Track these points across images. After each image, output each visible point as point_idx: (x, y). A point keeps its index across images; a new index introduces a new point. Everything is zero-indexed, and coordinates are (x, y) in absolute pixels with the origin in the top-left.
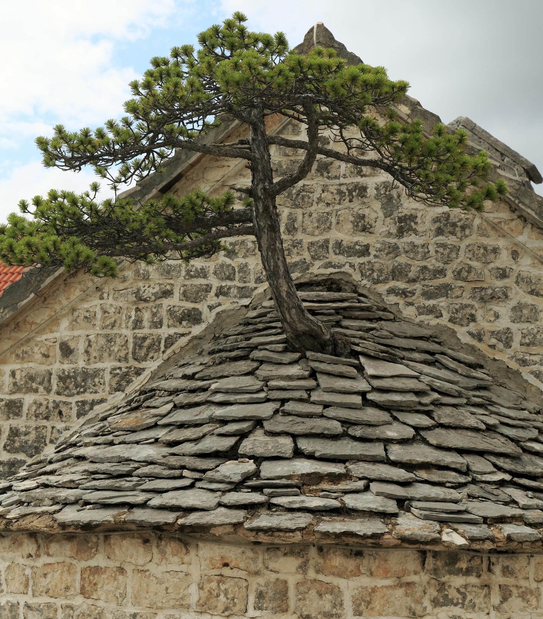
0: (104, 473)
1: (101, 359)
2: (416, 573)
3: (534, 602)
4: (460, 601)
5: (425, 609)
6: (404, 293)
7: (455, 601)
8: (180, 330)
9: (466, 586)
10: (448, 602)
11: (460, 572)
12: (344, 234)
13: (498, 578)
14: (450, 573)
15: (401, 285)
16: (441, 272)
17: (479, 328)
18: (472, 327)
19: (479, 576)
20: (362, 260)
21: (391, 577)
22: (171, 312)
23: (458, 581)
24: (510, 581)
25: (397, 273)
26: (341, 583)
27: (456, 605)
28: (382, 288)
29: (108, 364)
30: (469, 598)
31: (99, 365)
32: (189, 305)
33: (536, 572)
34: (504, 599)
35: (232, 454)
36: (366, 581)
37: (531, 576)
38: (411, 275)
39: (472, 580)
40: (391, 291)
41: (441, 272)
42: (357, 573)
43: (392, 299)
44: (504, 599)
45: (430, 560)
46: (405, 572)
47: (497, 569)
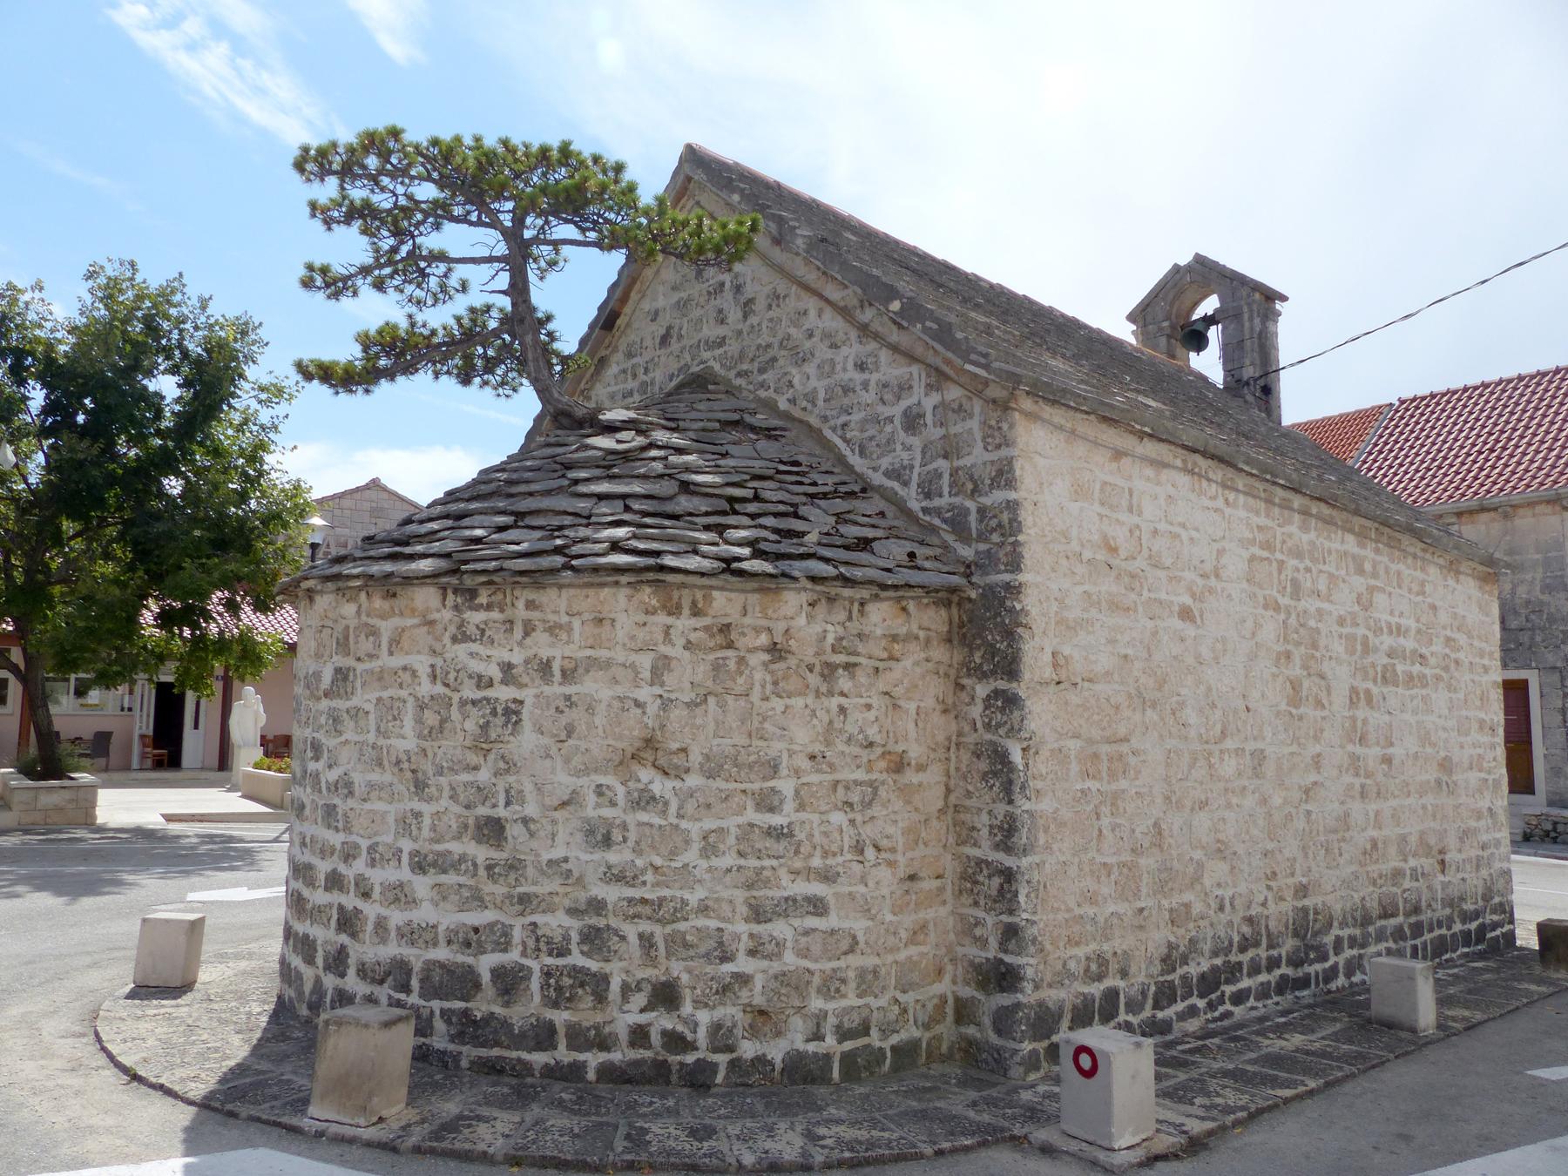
0: (596, 569)
3: (564, 636)
9: (486, 623)
12: (711, 331)
13: (521, 612)
14: (471, 609)
19: (502, 611)
20: (721, 351)
24: (535, 615)
27: (474, 641)
30: (488, 633)
34: (527, 634)
37: (563, 608)
39: (495, 615)
41: (769, 346)
44: (527, 634)
45: (450, 596)
47: (521, 604)
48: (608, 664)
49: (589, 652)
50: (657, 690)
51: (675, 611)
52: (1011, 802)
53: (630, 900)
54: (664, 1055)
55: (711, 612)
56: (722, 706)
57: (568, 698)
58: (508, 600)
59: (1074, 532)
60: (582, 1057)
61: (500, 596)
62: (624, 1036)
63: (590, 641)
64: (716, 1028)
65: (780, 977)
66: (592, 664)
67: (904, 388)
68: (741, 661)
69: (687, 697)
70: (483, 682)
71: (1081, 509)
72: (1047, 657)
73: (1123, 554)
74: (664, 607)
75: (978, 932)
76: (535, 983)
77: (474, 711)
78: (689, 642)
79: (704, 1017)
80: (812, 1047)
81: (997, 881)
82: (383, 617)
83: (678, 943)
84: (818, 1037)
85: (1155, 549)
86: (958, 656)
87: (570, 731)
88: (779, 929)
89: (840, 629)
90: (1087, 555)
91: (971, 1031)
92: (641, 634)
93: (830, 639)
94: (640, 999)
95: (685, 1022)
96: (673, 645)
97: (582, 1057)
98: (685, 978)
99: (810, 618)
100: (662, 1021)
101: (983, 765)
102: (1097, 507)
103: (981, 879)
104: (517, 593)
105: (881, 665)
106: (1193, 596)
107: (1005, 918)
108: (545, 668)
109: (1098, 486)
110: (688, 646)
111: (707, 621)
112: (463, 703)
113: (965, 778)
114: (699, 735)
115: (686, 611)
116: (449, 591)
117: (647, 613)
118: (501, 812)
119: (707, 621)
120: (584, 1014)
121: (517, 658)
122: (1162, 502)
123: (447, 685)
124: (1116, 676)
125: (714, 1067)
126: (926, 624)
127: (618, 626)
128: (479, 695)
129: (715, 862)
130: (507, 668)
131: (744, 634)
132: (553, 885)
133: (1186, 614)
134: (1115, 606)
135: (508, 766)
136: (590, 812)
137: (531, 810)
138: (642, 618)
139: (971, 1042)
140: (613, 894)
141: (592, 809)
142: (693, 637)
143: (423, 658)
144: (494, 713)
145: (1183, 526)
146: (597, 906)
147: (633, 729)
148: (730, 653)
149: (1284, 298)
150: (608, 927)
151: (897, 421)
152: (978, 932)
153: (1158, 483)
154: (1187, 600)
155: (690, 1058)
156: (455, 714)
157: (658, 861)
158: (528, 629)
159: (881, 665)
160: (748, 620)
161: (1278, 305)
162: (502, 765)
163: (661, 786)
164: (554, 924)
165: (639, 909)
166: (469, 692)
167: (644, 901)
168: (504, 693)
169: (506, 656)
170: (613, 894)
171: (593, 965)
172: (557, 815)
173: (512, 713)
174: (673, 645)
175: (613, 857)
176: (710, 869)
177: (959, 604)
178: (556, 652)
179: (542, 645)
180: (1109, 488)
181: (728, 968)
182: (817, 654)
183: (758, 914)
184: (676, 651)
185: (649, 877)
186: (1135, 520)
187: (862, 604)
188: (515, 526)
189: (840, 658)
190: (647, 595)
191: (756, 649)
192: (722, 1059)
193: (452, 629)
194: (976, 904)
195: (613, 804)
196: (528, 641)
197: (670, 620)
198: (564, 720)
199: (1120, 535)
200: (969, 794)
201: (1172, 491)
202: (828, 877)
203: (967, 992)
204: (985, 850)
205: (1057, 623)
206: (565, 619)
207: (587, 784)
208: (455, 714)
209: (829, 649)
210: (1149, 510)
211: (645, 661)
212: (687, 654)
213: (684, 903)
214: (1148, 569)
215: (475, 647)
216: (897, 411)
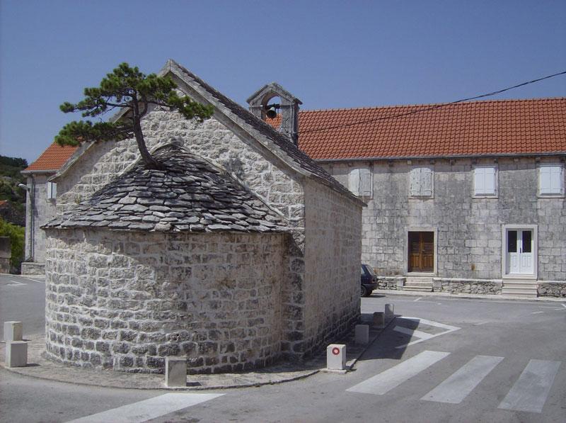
1: (105, 172)
3: (204, 249)
6: (196, 149)
8: (129, 162)
10: (173, 249)
11: (177, 240)
13: (191, 241)
15: (196, 146)
16: (208, 141)
18: (217, 159)
22: (126, 156)
23: (178, 242)
25: (195, 142)
26: (140, 244)
28: (190, 147)
29: (108, 174)
31: (105, 174)
32: (132, 154)
35: (116, 202)
36: (146, 243)
37: (203, 241)
40: (192, 148)
41: (208, 141)
43: (192, 150)
44: (193, 248)
48: (215, 257)
50: (229, 264)
52: (301, 290)
53: (223, 323)
54: (230, 364)
56: (244, 268)
57: (205, 267)
60: (210, 367)
62: (221, 360)
64: (243, 355)
65: (255, 341)
66: (212, 257)
67: (265, 168)
68: (248, 254)
69: (236, 266)
70: (179, 262)
75: (289, 325)
76: (197, 348)
77: (176, 271)
79: (240, 352)
80: (261, 358)
81: (296, 311)
82: (140, 241)
83: (233, 333)
84: (262, 356)
86: (284, 249)
87: (206, 276)
88: (254, 327)
91: (286, 351)
94: (225, 350)
95: (236, 354)
97: (210, 367)
98: (235, 343)
99: (262, 242)
100: (229, 355)
101: (292, 280)
103: (291, 311)
107: (299, 321)
108: (198, 258)
110: (236, 251)
111: (240, 244)
112: (173, 269)
113: (286, 283)
114: (239, 276)
118: (185, 300)
119: (240, 244)
120: (211, 354)
121: (190, 255)
123: (167, 263)
125: (242, 365)
128: (178, 266)
129: (242, 311)
130: (187, 258)
132: (202, 320)
135: (188, 287)
136: (212, 299)
137: (195, 299)
138: (224, 243)
139: (286, 355)
140: (218, 321)
141: (212, 298)
142: (238, 248)
143: (158, 255)
144: (183, 272)
146: (214, 325)
147: (222, 275)
149: (301, 103)
150: (217, 331)
151: (262, 177)
152: (289, 325)
155: (236, 364)
156: (170, 272)
157: (229, 312)
158: (193, 246)
160: (250, 243)
162: (185, 287)
163: (229, 291)
164: (201, 331)
165: (225, 325)
166: (175, 265)
167: (226, 323)
168: (186, 265)
169: (186, 255)
170: (218, 321)
171: (213, 342)
172: (203, 301)
173: (188, 271)
175: (217, 311)
176: (241, 313)
178: (202, 253)
179: (197, 251)
181: (245, 339)
183: (251, 324)
184: (233, 253)
185: (226, 316)
190: (227, 238)
192: (243, 363)
194: (289, 318)
195: (218, 296)
196: (193, 250)
198: (204, 273)
200: (287, 288)
202: (264, 313)
203: (285, 341)
204: (292, 303)
207: (211, 291)
208: (170, 272)
211: (225, 255)
213: (235, 322)
215: (176, 252)
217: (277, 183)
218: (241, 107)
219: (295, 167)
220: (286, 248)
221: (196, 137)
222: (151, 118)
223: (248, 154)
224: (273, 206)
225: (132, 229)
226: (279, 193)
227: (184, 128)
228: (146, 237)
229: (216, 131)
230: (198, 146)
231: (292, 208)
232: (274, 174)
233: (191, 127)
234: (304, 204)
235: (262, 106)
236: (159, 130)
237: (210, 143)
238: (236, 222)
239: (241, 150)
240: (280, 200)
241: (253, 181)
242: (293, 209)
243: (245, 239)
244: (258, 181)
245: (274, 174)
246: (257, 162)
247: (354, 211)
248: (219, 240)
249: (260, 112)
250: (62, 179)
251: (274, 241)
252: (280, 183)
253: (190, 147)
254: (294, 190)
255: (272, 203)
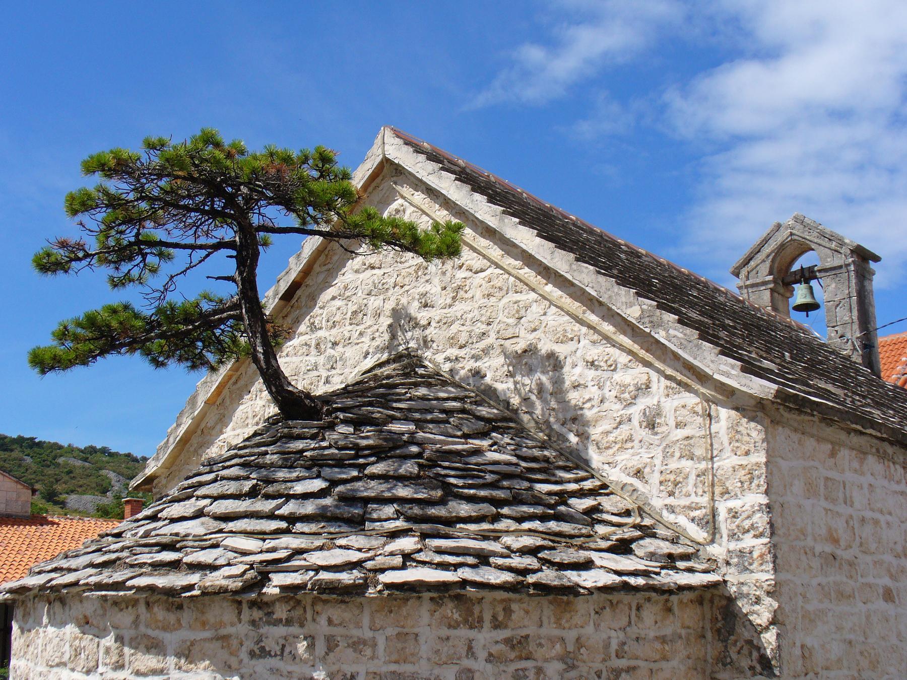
2: (232, 625)
4: (279, 653)
5: (241, 661)
7: (273, 653)
10: (264, 653)
13: (322, 627)
14: (269, 623)
17: (388, 313)
19: (302, 625)
21: (209, 629)
33: (372, 621)
38: (462, 341)
42: (179, 625)
46: (221, 624)
49: (393, 667)
51: (475, 624)
55: (511, 624)
58: (309, 615)
59: (809, 529)
61: (298, 612)
63: (394, 657)
67: (644, 388)
68: (539, 671)
71: (813, 505)
72: (797, 652)
73: (843, 543)
74: (466, 621)
78: (490, 655)
82: (166, 628)
85: (864, 536)
89: (621, 635)
90: (818, 549)
92: (445, 649)
93: (614, 646)
96: (476, 659)
99: (597, 626)
102: (823, 503)
104: (318, 608)
105: (655, 666)
106: (892, 576)
109: (822, 483)
115: (487, 624)
116: (245, 606)
117: (450, 627)
122: (866, 490)
124: (845, 663)
126: (687, 623)
127: (422, 640)
131: (540, 645)
133: (888, 595)
134: (843, 596)
142: (495, 649)
145: (881, 512)
148: (529, 664)
149: (877, 259)
151: (635, 422)
153: (862, 474)
154: (886, 581)
158: (331, 644)
159: (655, 666)
160: (544, 631)
161: (872, 265)
174: (476, 659)
177: (711, 601)
180: (830, 484)
182: (604, 660)
186: (850, 511)
187: (638, 608)
188: (287, 531)
189: (623, 663)
190: (450, 610)
191: (552, 658)
193: (249, 645)
197: (472, 634)
199: (840, 525)
201: (871, 479)
205: (803, 616)
206: (368, 634)
209: (613, 655)
210: (859, 499)
212: (489, 666)
214: (860, 555)
216: (636, 411)
217: (680, 433)
218: (591, 232)
219: (726, 371)
220: (720, 645)
221: (455, 328)
222: (348, 294)
223: (594, 353)
224: (671, 509)
225: (139, 589)
226: (686, 464)
227: (426, 306)
228: (187, 616)
229: (505, 300)
230: (462, 353)
231: (730, 510)
232: (670, 405)
233: (441, 302)
234: (767, 493)
235: (770, 278)
236: (369, 321)
237: (490, 340)
238: (492, 560)
239: (572, 346)
240: (690, 488)
241: (611, 438)
242: (734, 514)
243: (528, 619)
244: (624, 436)
245: (670, 405)
246: (618, 377)
247: (849, 476)
248: (423, 619)
249: (767, 295)
250: (164, 481)
251: (650, 622)
252: (686, 432)
253: (440, 358)
254: (740, 449)
255: (670, 501)
